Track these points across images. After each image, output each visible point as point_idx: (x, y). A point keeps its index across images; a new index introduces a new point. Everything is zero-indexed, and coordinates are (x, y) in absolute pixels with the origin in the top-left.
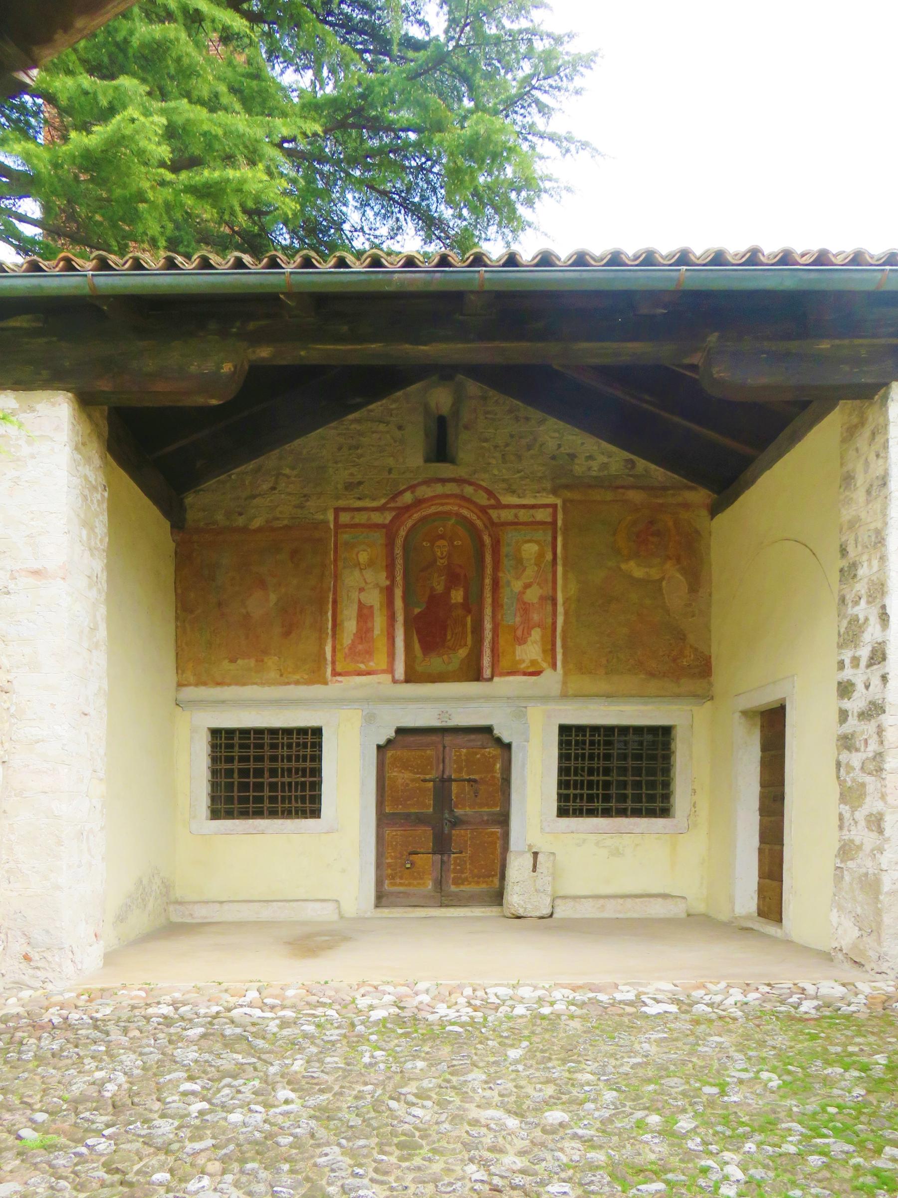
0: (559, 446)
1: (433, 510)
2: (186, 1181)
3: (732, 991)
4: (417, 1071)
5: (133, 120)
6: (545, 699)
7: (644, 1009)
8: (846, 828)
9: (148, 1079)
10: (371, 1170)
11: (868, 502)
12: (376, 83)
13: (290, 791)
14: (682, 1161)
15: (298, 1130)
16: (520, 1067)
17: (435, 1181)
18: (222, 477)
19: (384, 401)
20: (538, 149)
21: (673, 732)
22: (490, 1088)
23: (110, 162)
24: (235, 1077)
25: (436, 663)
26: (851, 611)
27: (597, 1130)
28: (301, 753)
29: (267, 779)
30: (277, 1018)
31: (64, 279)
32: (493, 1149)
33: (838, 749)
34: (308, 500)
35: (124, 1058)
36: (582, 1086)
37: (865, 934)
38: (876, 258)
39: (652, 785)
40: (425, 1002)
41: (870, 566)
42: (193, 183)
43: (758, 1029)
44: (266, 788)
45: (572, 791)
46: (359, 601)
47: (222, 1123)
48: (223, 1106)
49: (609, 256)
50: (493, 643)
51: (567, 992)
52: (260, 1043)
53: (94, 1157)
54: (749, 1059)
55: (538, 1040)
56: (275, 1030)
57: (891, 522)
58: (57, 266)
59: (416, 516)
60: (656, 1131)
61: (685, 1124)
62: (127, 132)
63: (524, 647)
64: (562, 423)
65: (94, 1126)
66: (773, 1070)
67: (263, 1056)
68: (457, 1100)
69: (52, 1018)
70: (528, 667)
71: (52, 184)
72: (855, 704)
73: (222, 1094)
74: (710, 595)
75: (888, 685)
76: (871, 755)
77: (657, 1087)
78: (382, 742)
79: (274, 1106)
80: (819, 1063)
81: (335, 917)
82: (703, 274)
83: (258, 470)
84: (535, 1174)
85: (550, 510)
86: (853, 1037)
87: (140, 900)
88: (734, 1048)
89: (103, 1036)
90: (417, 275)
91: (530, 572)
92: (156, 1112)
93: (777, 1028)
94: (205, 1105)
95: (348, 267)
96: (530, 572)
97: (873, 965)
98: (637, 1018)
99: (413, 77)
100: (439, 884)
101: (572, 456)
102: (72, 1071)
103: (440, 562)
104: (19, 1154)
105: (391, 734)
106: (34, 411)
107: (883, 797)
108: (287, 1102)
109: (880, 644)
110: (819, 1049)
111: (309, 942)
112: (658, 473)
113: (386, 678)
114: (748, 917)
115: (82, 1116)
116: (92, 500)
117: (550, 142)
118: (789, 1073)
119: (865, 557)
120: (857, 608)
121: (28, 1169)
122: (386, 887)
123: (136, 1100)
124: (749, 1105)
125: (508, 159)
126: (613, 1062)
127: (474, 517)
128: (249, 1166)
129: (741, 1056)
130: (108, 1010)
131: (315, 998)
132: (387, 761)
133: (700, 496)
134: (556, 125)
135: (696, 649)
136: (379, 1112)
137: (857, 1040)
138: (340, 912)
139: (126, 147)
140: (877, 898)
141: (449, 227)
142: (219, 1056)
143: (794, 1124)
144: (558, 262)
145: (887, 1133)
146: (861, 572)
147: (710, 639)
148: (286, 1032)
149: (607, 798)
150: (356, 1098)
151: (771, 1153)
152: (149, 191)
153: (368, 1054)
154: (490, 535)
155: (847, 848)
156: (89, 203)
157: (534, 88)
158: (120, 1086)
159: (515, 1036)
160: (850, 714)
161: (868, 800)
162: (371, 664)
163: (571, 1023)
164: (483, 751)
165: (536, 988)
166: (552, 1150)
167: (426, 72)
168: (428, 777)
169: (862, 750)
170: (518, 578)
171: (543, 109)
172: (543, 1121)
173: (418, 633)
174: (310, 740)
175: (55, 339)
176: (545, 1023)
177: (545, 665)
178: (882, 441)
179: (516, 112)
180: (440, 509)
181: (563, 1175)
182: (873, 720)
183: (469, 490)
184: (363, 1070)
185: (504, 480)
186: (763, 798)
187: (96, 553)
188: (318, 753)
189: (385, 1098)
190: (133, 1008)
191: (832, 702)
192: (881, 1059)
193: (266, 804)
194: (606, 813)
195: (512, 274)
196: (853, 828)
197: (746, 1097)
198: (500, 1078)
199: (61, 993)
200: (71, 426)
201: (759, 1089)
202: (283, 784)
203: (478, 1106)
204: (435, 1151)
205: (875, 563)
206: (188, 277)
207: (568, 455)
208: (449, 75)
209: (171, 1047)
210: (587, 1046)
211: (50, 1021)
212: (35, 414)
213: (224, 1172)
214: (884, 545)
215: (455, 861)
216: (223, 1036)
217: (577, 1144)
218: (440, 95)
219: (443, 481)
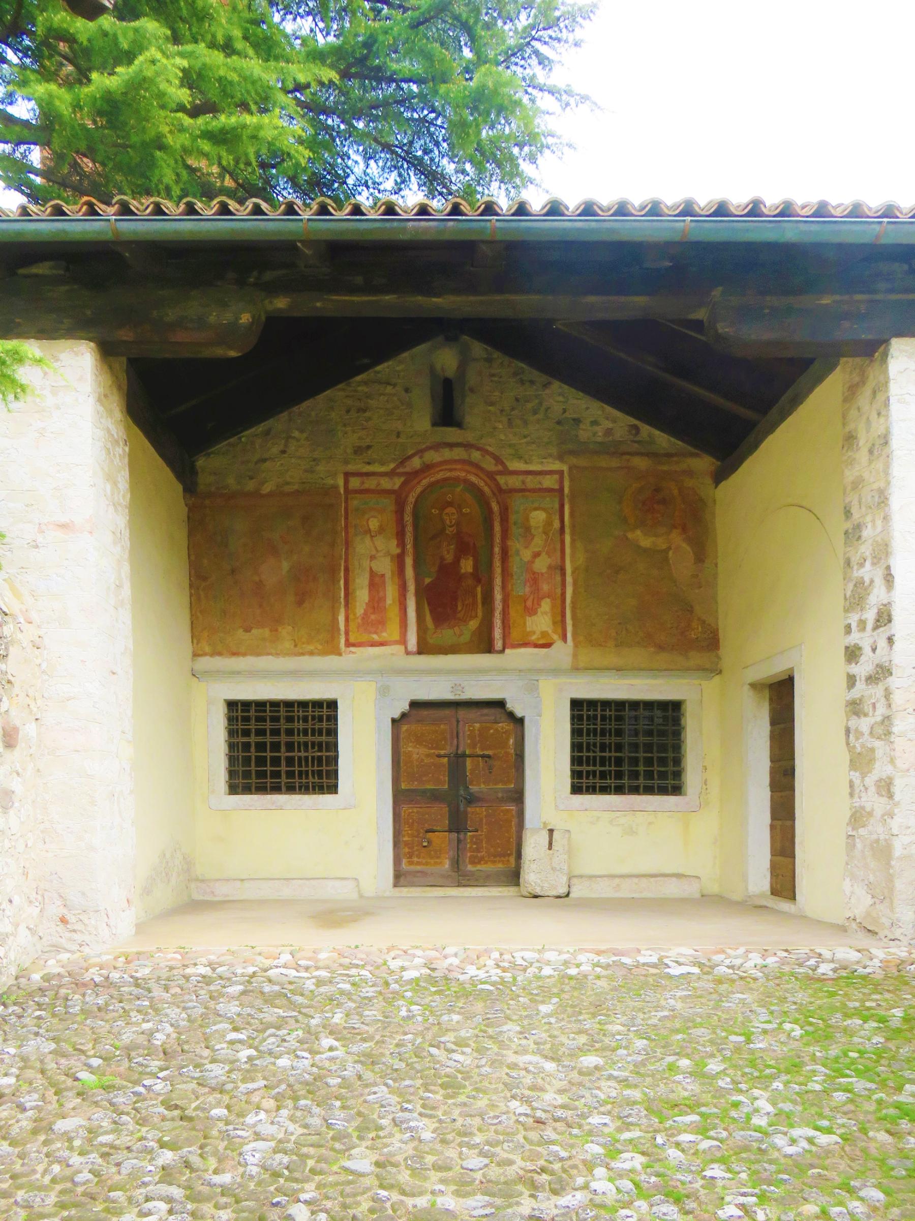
0: (565, 411)
1: (440, 476)
2: (244, 1116)
3: (750, 955)
4: (454, 1023)
5: (153, 62)
6: (556, 672)
7: (667, 970)
8: (856, 796)
9: (195, 1030)
10: (419, 1106)
11: (870, 462)
12: (380, 31)
13: (307, 766)
14: (714, 1097)
15: (345, 1073)
16: (553, 1020)
17: (481, 1115)
18: (232, 440)
19: (390, 363)
20: (539, 103)
21: (683, 707)
22: (526, 1038)
23: (129, 105)
24: (278, 1028)
25: (447, 635)
26: (857, 573)
27: (631, 1072)
28: (317, 727)
29: (283, 754)
30: (313, 977)
31: (87, 223)
32: (534, 1088)
33: (847, 715)
34: (318, 465)
35: (168, 1011)
36: (614, 1035)
37: (877, 901)
38: (874, 210)
39: (663, 761)
40: (455, 964)
41: (874, 526)
42: (210, 128)
43: (778, 988)
44: (283, 763)
45: (585, 768)
46: (371, 569)
47: (271, 1067)
48: (270, 1053)
49: (616, 206)
50: (504, 615)
51: (591, 956)
52: (299, 999)
53: (153, 1096)
54: (772, 1012)
55: (567, 997)
56: (313, 987)
57: (894, 482)
58: (80, 210)
59: (425, 482)
60: (687, 1073)
61: (714, 1066)
62: (149, 73)
63: (535, 618)
64: (566, 387)
65: (148, 1070)
66: (795, 1022)
67: (304, 1010)
68: (495, 1048)
69: (94, 977)
70: (538, 639)
71: (73, 128)
72: (862, 669)
73: (268, 1042)
74: (716, 565)
75: (894, 647)
76: (879, 719)
77: (685, 1036)
78: (397, 715)
79: (320, 1053)
80: (839, 1015)
81: (355, 896)
82: (706, 225)
83: (267, 433)
84: (576, 1108)
85: (556, 477)
86: (870, 994)
87: (164, 874)
88: (756, 1004)
89: (146, 993)
90: (431, 224)
91: (538, 542)
92: (206, 1058)
93: (797, 987)
94: (252, 1052)
95: (363, 214)
96: (538, 542)
97: (886, 932)
98: (661, 978)
99: (416, 25)
100: (456, 864)
101: (577, 421)
102: (119, 1023)
103: (450, 531)
104: (79, 1094)
105: (406, 707)
106: (58, 360)
107: (892, 761)
108: (331, 1049)
109: (885, 605)
110: (838, 1004)
111: (331, 916)
112: (663, 440)
113: (400, 649)
114: (762, 895)
115: (135, 1061)
116: (114, 454)
117: (550, 95)
118: (811, 1024)
119: (868, 518)
120: (862, 570)
121: (89, 1106)
122: (404, 866)
123: (186, 1047)
124: (774, 1051)
125: (513, 112)
126: (641, 1015)
127: (482, 484)
128: (302, 1102)
129: (764, 1010)
130: (147, 971)
131: (348, 960)
132: (402, 736)
133: (704, 463)
134: (556, 78)
135: (704, 622)
136: (421, 1057)
137: (874, 997)
138: (359, 891)
139: (146, 90)
140: (888, 865)
141: (451, 182)
142: (260, 1010)
143: (819, 1067)
144: (566, 212)
145: (907, 1073)
146: (866, 533)
147: (717, 611)
148: (322, 989)
149: (619, 775)
150: (397, 1045)
151: (797, 1090)
152: (168, 135)
153: (404, 1009)
154: (498, 503)
155: (858, 815)
156: (102, 148)
157: (533, 38)
158: (168, 1036)
159: (545, 993)
160: (858, 679)
161: (877, 765)
162: (384, 634)
163: (599, 983)
164: (496, 726)
165: (560, 953)
166: (590, 1089)
167: (426, 20)
168: (442, 752)
169: (871, 714)
170: (526, 547)
171: (543, 61)
172: (579, 1065)
173: (429, 604)
174: (324, 714)
175: (76, 287)
176: (573, 983)
177: (555, 637)
178: (883, 399)
179: (516, 64)
180: (448, 474)
181: (602, 1109)
182: (880, 684)
183: (476, 455)
184: (401, 1022)
185: (510, 446)
186: (773, 773)
187: (120, 508)
188: (333, 726)
189: (426, 1046)
190: (171, 968)
191: (840, 667)
192: (898, 1013)
193: (284, 779)
194: (619, 790)
195: (524, 223)
196: (863, 794)
197: (771, 1045)
198: (534, 1029)
199: (99, 956)
200: (94, 377)
201: (783, 1038)
202: (300, 758)
203: (516, 1053)
204: (478, 1090)
205: (879, 523)
206: (208, 222)
207: (574, 420)
208: (451, 24)
209: (213, 1002)
210: (615, 1002)
211: (92, 979)
212: (59, 363)
213: (278, 1108)
214: (887, 505)
215: (471, 840)
216: (262, 993)
217: (613, 1083)
218: (442, 44)
219: (451, 446)
